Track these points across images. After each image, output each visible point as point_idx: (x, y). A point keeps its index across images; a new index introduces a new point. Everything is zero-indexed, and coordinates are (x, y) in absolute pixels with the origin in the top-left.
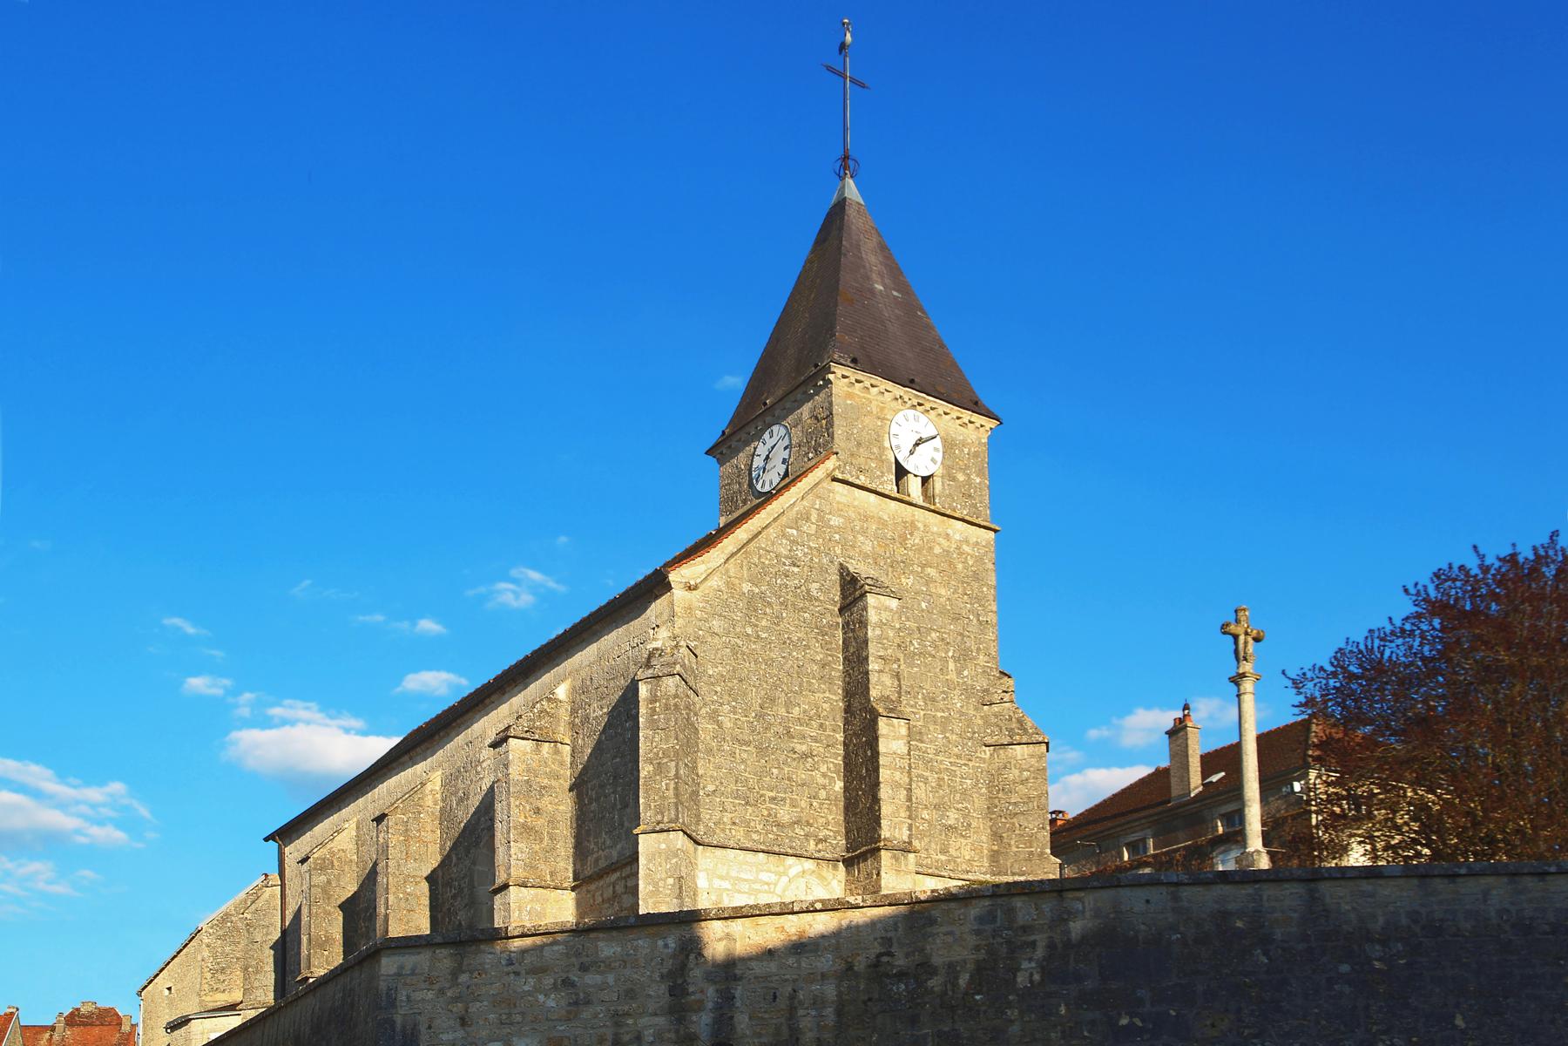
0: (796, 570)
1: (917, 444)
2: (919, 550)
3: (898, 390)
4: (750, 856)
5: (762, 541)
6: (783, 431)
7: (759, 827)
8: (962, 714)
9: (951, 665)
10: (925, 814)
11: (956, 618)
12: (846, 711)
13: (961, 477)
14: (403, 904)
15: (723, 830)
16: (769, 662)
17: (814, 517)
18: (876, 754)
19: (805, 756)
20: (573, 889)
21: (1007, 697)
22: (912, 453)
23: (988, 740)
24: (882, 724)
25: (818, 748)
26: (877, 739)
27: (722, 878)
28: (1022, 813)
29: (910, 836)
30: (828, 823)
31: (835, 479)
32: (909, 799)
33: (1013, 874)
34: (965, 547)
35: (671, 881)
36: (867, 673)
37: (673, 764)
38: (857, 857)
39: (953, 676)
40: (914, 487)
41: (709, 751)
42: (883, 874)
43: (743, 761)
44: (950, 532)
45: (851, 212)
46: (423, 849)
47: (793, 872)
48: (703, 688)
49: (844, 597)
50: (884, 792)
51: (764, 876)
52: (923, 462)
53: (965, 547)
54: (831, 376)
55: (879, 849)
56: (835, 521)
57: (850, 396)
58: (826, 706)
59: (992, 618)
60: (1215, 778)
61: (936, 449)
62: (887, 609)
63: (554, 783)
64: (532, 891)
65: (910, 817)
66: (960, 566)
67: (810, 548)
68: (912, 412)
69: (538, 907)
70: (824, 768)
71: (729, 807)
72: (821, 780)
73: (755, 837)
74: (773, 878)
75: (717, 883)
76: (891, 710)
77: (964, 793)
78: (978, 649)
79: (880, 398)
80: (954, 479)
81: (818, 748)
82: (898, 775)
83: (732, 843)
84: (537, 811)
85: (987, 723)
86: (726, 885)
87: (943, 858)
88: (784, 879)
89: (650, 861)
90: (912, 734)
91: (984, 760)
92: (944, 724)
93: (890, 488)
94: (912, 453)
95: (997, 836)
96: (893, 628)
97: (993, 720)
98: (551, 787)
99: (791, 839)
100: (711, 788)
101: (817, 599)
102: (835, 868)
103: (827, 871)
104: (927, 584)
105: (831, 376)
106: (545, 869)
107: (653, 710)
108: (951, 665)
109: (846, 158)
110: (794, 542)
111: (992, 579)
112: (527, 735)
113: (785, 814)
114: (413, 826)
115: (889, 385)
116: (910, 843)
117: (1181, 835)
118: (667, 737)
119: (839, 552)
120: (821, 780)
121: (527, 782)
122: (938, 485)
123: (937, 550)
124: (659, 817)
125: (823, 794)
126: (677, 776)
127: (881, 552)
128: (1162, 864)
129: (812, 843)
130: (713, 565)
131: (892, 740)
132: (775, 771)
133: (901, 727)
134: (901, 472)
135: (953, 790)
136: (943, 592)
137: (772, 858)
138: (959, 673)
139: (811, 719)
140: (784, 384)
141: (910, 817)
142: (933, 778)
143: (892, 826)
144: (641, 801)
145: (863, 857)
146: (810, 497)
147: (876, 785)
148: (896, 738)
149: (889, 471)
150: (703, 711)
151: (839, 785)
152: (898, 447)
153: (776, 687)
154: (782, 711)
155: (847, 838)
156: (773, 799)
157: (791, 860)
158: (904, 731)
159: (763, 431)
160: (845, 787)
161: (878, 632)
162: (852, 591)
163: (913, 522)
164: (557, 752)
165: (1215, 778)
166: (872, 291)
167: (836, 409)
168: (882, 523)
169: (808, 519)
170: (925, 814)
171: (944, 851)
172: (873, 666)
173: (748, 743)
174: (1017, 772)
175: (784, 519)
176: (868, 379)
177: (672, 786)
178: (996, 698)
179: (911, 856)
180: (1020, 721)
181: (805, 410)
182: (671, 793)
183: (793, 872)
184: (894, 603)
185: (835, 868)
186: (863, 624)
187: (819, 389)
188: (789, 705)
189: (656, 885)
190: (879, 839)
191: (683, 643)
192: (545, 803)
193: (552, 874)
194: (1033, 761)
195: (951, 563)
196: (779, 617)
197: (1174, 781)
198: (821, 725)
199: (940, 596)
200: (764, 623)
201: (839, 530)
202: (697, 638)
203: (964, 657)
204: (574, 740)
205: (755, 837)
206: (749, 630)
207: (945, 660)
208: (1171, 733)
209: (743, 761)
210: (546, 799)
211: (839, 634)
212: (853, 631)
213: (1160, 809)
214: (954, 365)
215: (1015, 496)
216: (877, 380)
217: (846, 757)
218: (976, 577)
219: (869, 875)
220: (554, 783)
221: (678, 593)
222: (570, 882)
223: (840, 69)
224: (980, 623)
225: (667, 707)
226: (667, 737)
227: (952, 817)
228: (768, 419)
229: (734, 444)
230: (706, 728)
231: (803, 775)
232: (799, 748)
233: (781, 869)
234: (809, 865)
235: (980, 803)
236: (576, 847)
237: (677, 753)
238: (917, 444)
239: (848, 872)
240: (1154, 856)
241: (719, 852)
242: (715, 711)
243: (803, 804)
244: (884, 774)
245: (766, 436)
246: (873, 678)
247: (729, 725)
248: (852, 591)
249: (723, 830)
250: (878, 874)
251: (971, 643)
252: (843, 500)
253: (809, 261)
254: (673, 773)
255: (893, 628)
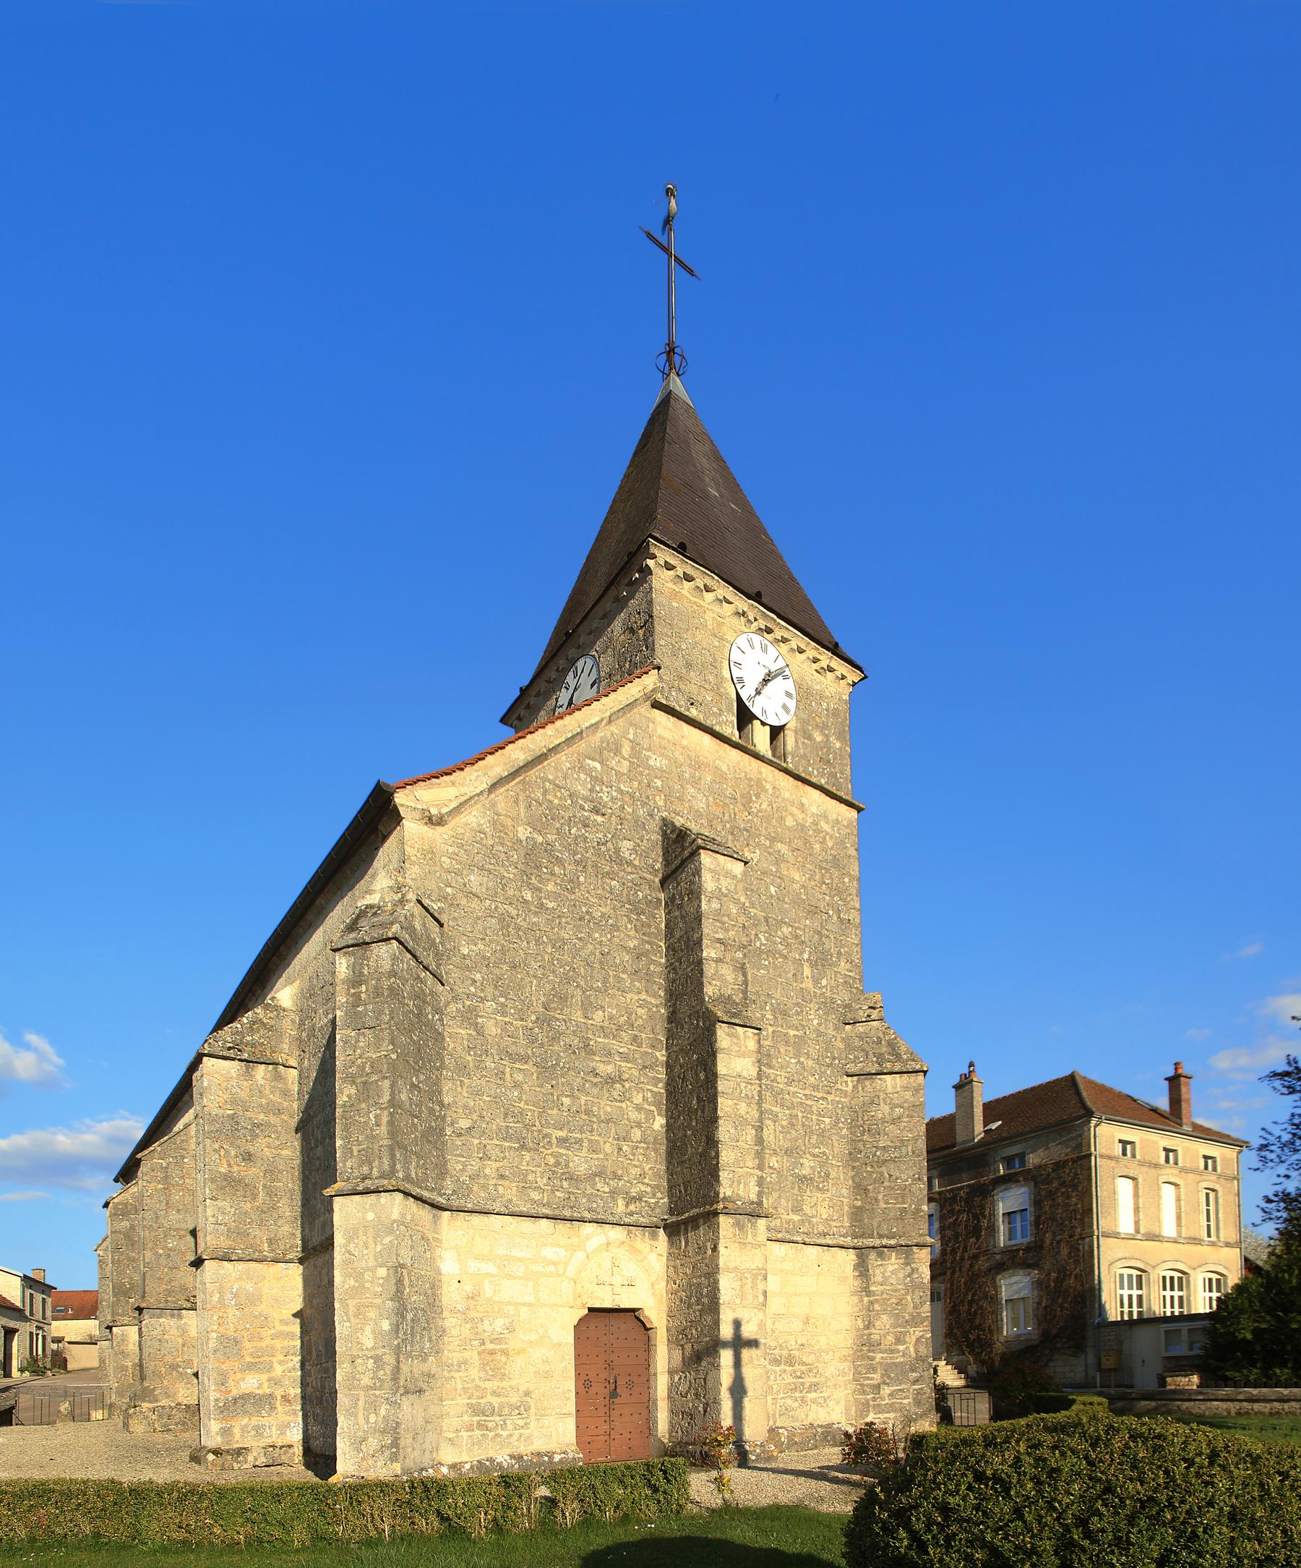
0: (599, 819)
1: (766, 681)
2: (768, 819)
3: (742, 603)
4: (526, 1224)
5: (548, 769)
6: (590, 662)
7: (542, 1182)
8: (820, 1034)
9: (807, 971)
10: (773, 1162)
11: (813, 911)
12: (670, 1020)
13: (818, 738)
14: (163, 1261)
15: (484, 1187)
16: (559, 944)
17: (626, 751)
18: (712, 1077)
19: (611, 1081)
20: (301, 1261)
21: (875, 1014)
22: (758, 693)
23: (851, 1068)
24: (722, 1032)
25: (629, 1070)
26: (713, 1055)
27: (481, 1258)
28: (893, 1160)
29: (760, 1194)
30: (643, 1175)
31: (657, 705)
32: (760, 1141)
33: (881, 1236)
34: (822, 823)
35: (382, 1272)
36: (700, 962)
37: (387, 1083)
38: (685, 1222)
39: (808, 984)
40: (761, 738)
41: (462, 1069)
42: (721, 1248)
43: (517, 1085)
44: (804, 801)
45: (675, 408)
46: (188, 1199)
47: (592, 1244)
48: (451, 972)
49: (667, 862)
50: (724, 1131)
51: (549, 1253)
52: (773, 706)
53: (822, 823)
54: (650, 563)
55: (716, 1214)
56: (656, 761)
57: (675, 595)
58: (641, 1011)
59: (854, 916)
60: (994, 1126)
61: (788, 695)
62: (728, 874)
63: (273, 1119)
64: (240, 1266)
65: (760, 1167)
66: (817, 846)
67: (621, 792)
68: (757, 639)
69: (250, 1287)
70: (638, 1099)
71: (494, 1152)
72: (634, 1115)
73: (535, 1195)
74: (562, 1253)
75: (473, 1266)
76: (734, 1015)
77: (822, 1134)
78: (839, 953)
79: (716, 608)
80: (810, 737)
81: (629, 1070)
82: (743, 1108)
83: (497, 1206)
84: (248, 1157)
85: (849, 1046)
86: (489, 1268)
87: (796, 1218)
88: (580, 1255)
89: (350, 1239)
90: (763, 1059)
91: (845, 1094)
92: (798, 1045)
93: (731, 731)
94: (758, 693)
95: (860, 1189)
96: (736, 901)
97: (857, 1043)
98: (269, 1124)
99: (590, 1198)
100: (464, 1124)
101: (630, 863)
102: (654, 1236)
103: (642, 1242)
104: (777, 863)
105: (650, 563)
106: (260, 1236)
107: (357, 996)
108: (807, 971)
109: (671, 351)
110: (596, 780)
111: (854, 869)
112: (231, 1054)
113: (580, 1162)
114: (175, 1173)
115: (728, 592)
116: (760, 1203)
117: (964, 1176)
118: (379, 1039)
119: (661, 803)
120: (634, 1115)
121: (232, 1117)
122: (790, 739)
123: (790, 822)
124: (365, 1170)
125: (637, 1134)
126: (393, 1103)
127: (718, 812)
128: (946, 1200)
129: (621, 1202)
130: (470, 790)
131: (735, 1057)
132: (566, 1101)
133: (748, 1039)
134: (745, 717)
135: (808, 1131)
136: (797, 877)
137: (561, 1226)
138: (816, 982)
139: (620, 1028)
140: (595, 620)
141: (760, 1167)
142: (783, 1115)
143: (736, 1179)
144: (339, 1143)
145: (693, 1223)
146: (621, 722)
147: (712, 1120)
148: (743, 1055)
149: (729, 710)
150: (452, 1008)
151: (659, 1122)
152: (741, 680)
153: (567, 980)
154: (578, 1016)
155: (670, 1196)
156: (562, 1141)
157: (589, 1228)
158: (752, 1045)
159: (565, 672)
160: (669, 1127)
161: (715, 905)
162: (680, 851)
163: (759, 782)
164: (278, 1077)
165: (994, 1126)
166: (706, 496)
167: (657, 610)
168: (720, 776)
169: (617, 752)
170: (773, 1162)
171: (797, 1209)
172: (709, 952)
173: (524, 1059)
174: (886, 1109)
175: (582, 746)
176: (702, 577)
177: (385, 1119)
178: (861, 1015)
179: (762, 1223)
180: (891, 1044)
181: (617, 626)
182: (384, 1129)
183: (592, 1244)
184: (738, 868)
185: (654, 1236)
186: (695, 893)
187: (634, 585)
188: (587, 1007)
189: (359, 1277)
190: (716, 1199)
191: (411, 896)
192: (262, 1146)
193: (270, 1242)
194: (908, 1095)
195: (806, 842)
196: (574, 882)
197: (959, 1129)
198: (635, 1038)
199: (793, 881)
200: (550, 887)
201: (661, 774)
202: (444, 898)
203: (822, 962)
204: (301, 1062)
205: (535, 1195)
206: (528, 896)
207: (799, 963)
208: (957, 1087)
209: (517, 1085)
210: (262, 1142)
211: (661, 914)
212: (680, 907)
213: (946, 1152)
214: (808, 602)
215: (880, 769)
216: (713, 581)
217: (670, 1084)
218: (836, 862)
219: (702, 1249)
220: (273, 1119)
221: (411, 828)
222: (297, 1253)
223: (665, 245)
224: (841, 920)
225: (377, 992)
226: (379, 1039)
227: (807, 1166)
228: (572, 652)
229: (532, 700)
230: (456, 1035)
231: (608, 1108)
232: (602, 1068)
233: (575, 1241)
234: (617, 1233)
235: (839, 1147)
236: (303, 1205)
237: (393, 1066)
238: (766, 681)
239: (671, 1243)
240: (939, 1193)
241: (476, 1219)
242: (472, 1010)
243: (608, 1148)
244: (724, 1105)
245: (570, 678)
246: (709, 969)
247: (494, 1031)
248: (680, 851)
249: (484, 1187)
250: (715, 1249)
251: (830, 945)
252: (668, 735)
253: (626, 476)
254: (386, 1098)
255: (736, 901)
